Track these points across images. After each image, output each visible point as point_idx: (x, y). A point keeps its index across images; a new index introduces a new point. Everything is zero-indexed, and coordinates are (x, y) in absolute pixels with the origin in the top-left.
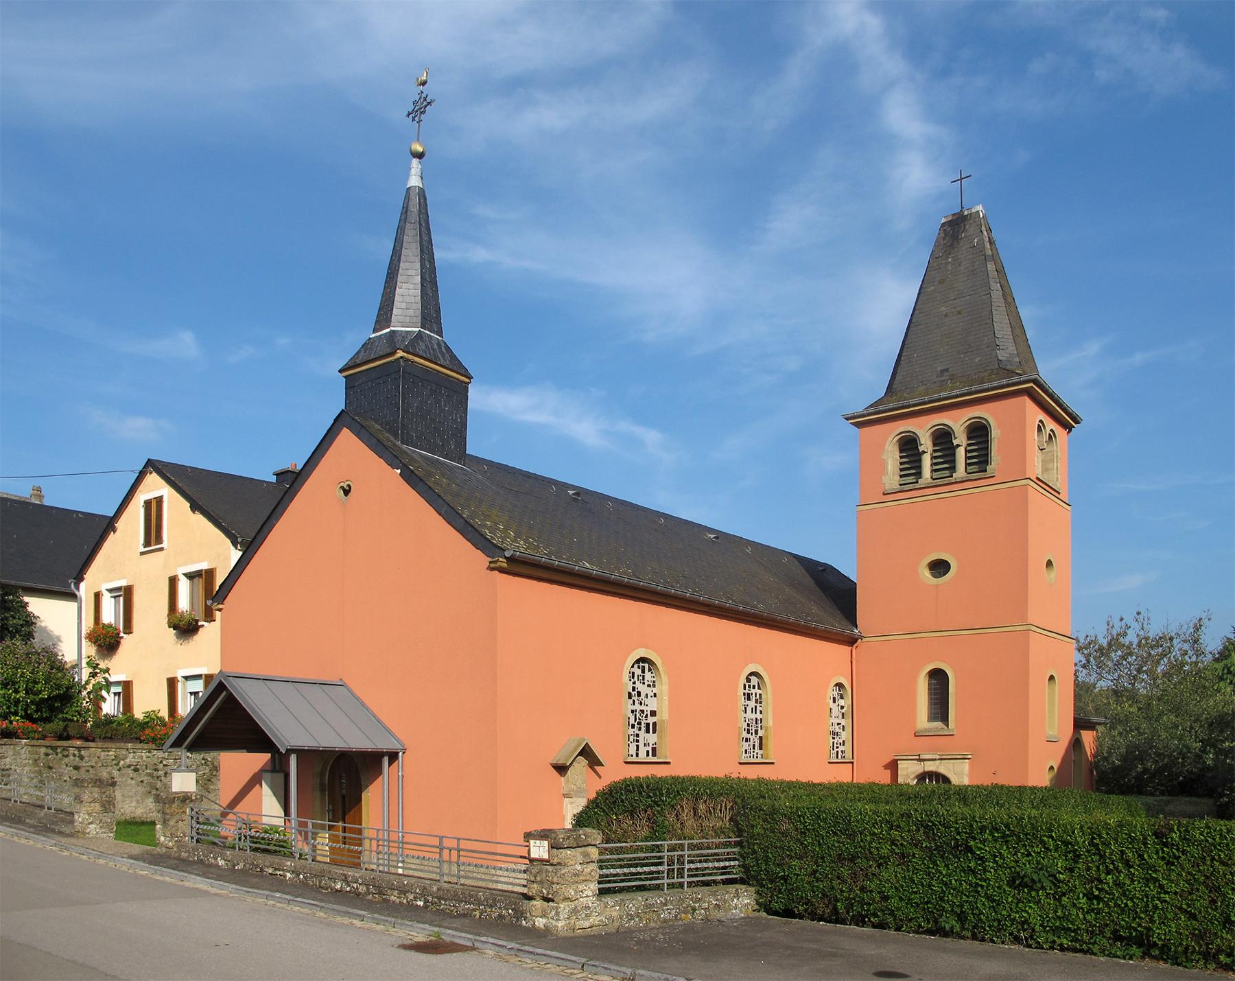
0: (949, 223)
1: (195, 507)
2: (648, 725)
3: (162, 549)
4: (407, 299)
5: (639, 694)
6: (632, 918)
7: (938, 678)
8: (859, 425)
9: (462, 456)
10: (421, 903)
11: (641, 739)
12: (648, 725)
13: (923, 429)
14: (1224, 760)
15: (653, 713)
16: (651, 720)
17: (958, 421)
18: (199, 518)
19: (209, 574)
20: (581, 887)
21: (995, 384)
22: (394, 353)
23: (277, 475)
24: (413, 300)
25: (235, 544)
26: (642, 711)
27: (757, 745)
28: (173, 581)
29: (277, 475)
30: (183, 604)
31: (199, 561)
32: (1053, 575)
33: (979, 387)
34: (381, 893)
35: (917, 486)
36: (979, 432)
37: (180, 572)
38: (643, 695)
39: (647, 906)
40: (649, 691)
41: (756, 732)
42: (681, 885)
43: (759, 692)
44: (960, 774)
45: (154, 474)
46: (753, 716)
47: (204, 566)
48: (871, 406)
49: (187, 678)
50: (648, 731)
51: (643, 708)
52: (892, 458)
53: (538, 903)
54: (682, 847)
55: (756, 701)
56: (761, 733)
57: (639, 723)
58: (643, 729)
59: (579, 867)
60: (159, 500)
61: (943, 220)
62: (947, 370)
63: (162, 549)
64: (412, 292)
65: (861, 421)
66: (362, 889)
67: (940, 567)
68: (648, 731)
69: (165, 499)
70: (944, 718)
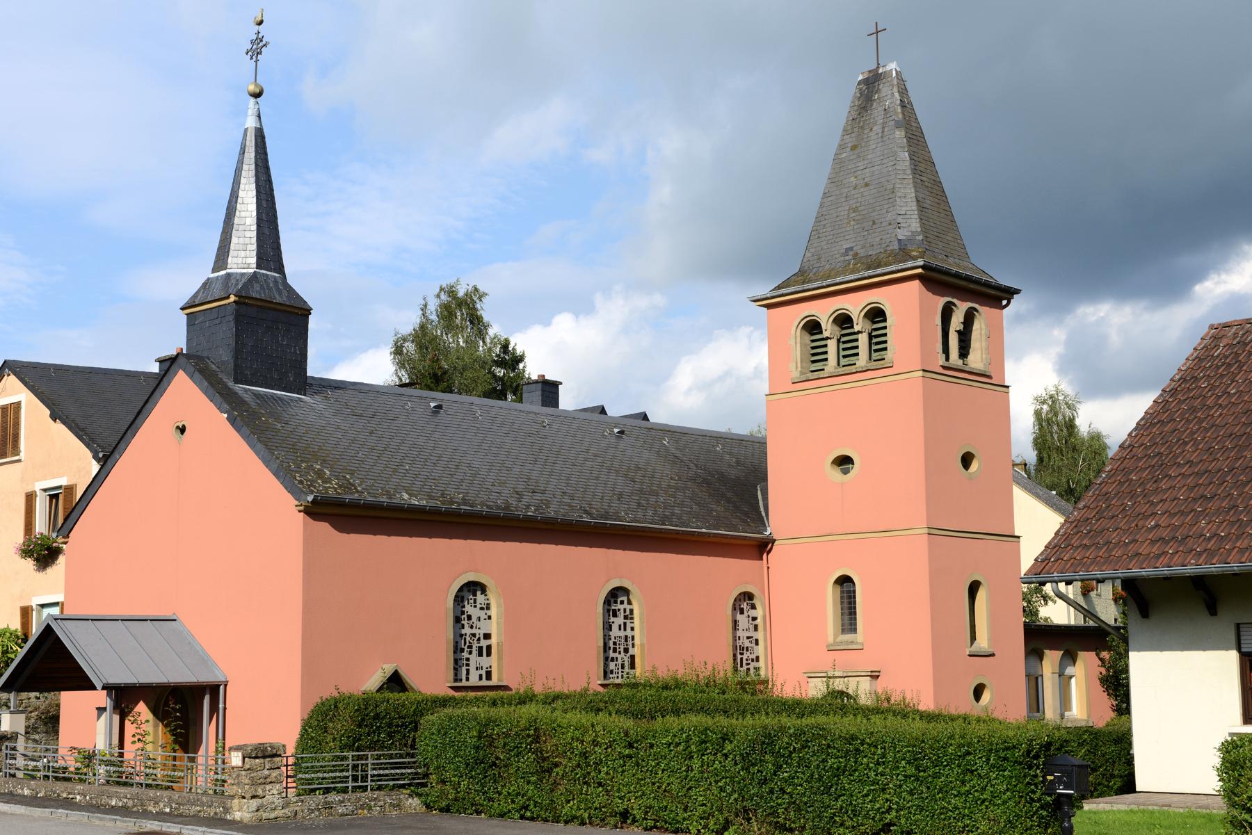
0: (866, 81)
1: (54, 417)
2: (480, 649)
3: (19, 461)
5: (469, 617)
8: (769, 306)
9: (303, 384)
10: (168, 810)
11: (472, 663)
12: (480, 649)
13: (824, 311)
15: (487, 636)
16: (484, 643)
17: (855, 305)
18: (60, 429)
19: (70, 489)
20: (268, 787)
21: (894, 268)
22: (228, 297)
23: (161, 361)
24: (247, 241)
25: (95, 457)
26: (474, 635)
27: (627, 664)
28: (30, 498)
29: (161, 361)
30: (41, 526)
31: (58, 476)
32: (835, 474)
33: (872, 272)
34: (142, 805)
36: (876, 315)
37: (38, 486)
38: (474, 619)
39: (326, 803)
40: (482, 614)
41: (626, 651)
42: (364, 789)
43: (628, 607)
44: (863, 690)
45: (12, 377)
46: (622, 634)
47: (63, 481)
48: (779, 287)
49: (43, 606)
50: (480, 654)
51: (474, 631)
52: (796, 342)
53: (236, 801)
55: (626, 617)
56: (631, 652)
57: (470, 647)
58: (475, 652)
59: (267, 772)
60: (17, 406)
61: (861, 78)
62: (851, 249)
63: (19, 461)
66: (130, 803)
67: (844, 462)
68: (480, 654)
69: (23, 405)
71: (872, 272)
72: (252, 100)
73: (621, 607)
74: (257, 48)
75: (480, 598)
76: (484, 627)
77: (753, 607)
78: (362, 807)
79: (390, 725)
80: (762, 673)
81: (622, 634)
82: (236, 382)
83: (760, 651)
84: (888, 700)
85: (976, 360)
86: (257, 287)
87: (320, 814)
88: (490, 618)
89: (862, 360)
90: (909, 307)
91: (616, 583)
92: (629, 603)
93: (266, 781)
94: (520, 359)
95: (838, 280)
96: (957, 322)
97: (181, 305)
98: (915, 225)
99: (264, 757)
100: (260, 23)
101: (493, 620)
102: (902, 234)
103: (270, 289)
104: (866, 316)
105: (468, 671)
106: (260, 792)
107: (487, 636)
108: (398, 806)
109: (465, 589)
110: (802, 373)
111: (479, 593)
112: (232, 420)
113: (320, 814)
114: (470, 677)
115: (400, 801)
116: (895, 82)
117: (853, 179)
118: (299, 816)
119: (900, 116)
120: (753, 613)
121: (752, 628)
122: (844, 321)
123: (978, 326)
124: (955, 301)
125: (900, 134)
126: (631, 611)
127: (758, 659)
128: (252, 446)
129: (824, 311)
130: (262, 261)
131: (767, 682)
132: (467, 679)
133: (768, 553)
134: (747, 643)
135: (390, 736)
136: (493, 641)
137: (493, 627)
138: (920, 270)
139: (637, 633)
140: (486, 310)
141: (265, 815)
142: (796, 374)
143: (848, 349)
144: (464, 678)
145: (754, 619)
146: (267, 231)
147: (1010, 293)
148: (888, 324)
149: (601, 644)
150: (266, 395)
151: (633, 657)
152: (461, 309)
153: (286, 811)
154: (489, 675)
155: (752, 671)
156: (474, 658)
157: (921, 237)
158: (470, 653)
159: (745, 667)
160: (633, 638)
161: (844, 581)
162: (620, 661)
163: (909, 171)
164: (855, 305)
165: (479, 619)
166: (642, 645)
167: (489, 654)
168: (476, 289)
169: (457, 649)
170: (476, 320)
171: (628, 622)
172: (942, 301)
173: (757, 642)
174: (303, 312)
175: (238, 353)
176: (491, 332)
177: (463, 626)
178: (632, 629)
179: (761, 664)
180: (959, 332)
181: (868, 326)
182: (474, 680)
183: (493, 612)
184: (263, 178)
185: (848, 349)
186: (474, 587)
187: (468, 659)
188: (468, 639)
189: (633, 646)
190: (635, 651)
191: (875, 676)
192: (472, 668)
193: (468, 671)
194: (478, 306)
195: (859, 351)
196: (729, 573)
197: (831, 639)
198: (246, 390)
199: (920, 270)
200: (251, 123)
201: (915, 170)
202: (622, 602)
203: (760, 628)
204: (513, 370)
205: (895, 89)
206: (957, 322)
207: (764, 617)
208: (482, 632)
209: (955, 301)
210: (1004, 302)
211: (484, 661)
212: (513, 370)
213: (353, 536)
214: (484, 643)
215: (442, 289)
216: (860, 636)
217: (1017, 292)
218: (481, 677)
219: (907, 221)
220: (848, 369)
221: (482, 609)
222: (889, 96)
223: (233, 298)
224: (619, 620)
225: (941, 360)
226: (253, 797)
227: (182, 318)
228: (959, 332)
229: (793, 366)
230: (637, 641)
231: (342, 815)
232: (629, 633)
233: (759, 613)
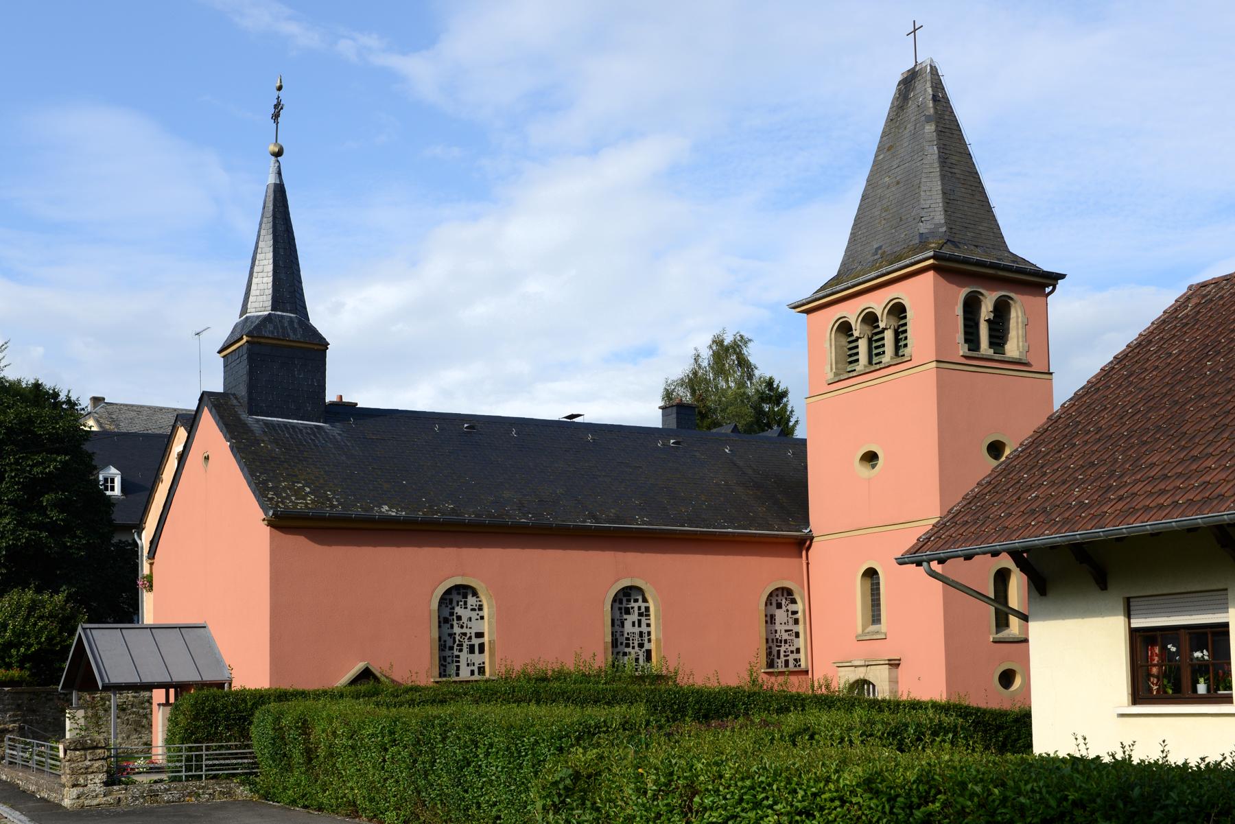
4: (261, 287)
6: (137, 799)
7: (871, 574)
8: (808, 312)
13: (851, 311)
14: (1177, 653)
15: (480, 635)
16: (476, 642)
17: (878, 302)
20: (90, 777)
21: (907, 262)
22: (241, 338)
23: (803, 442)
26: (465, 634)
29: (803, 442)
32: (864, 471)
33: (896, 266)
35: (854, 374)
36: (898, 310)
38: (464, 619)
40: (474, 615)
41: (641, 646)
43: (643, 605)
48: (822, 288)
51: (464, 630)
52: (828, 345)
54: (200, 749)
55: (640, 615)
56: (647, 646)
57: (461, 645)
62: (880, 248)
64: (265, 280)
65: (809, 307)
67: (870, 458)
70: (876, 619)
71: (896, 266)
72: (273, 158)
73: (636, 605)
75: (471, 600)
76: (476, 627)
77: (794, 601)
78: (190, 795)
79: (227, 718)
80: (803, 663)
81: (636, 630)
82: (251, 413)
83: (801, 643)
84: (827, 687)
85: (1013, 348)
86: (270, 327)
87: (145, 801)
88: (482, 618)
89: (886, 359)
90: (922, 295)
91: (626, 582)
92: (645, 600)
93: (87, 771)
94: (785, 394)
95: (861, 279)
96: (986, 310)
97: (218, 349)
98: (940, 217)
99: (85, 749)
101: (484, 620)
102: (923, 228)
103: (283, 327)
104: (890, 312)
107: (480, 635)
108: (229, 793)
109: (454, 592)
110: (836, 374)
111: (470, 597)
112: (232, 448)
113: (145, 801)
115: (231, 789)
116: (929, 78)
117: (887, 179)
118: (123, 803)
119: (932, 111)
120: (792, 607)
121: (791, 621)
122: (870, 319)
123: (1016, 316)
124: (1012, 295)
125: (930, 128)
126: (647, 609)
127: (798, 651)
128: (242, 470)
130: (277, 303)
131: (806, 672)
132: (458, 675)
133: (808, 549)
134: (785, 636)
135: (228, 728)
136: (486, 639)
137: (485, 627)
138: (931, 261)
139: (652, 629)
140: (753, 354)
141: (86, 803)
142: (830, 376)
144: (453, 672)
145: (795, 613)
146: (283, 276)
147: (1054, 278)
148: (907, 320)
149: (609, 639)
150: (279, 424)
151: (649, 652)
153: (108, 798)
154: (481, 670)
155: (791, 663)
156: (464, 656)
157: (944, 229)
158: (461, 650)
159: (783, 659)
160: (649, 633)
161: (871, 574)
162: (633, 656)
163: (936, 165)
164: (878, 302)
165: (470, 619)
166: (657, 640)
167: (482, 650)
168: (742, 337)
169: (443, 646)
170: (743, 363)
171: (643, 619)
172: (963, 292)
173: (797, 635)
175: (251, 387)
176: (757, 373)
177: (452, 626)
178: (648, 625)
179: (802, 656)
180: (988, 321)
181: (894, 323)
182: (465, 674)
183: (485, 612)
184: (281, 228)
186: (464, 591)
187: (458, 657)
188: (457, 638)
189: (649, 641)
190: (653, 646)
191: (894, 664)
192: (463, 664)
193: (458, 668)
194: (744, 351)
195: (886, 349)
196: (767, 571)
197: (860, 630)
198: (258, 421)
199: (931, 261)
200: (272, 179)
201: (944, 160)
202: (636, 601)
203: (801, 622)
204: (778, 405)
205: (929, 84)
206: (986, 310)
207: (804, 611)
208: (473, 631)
209: (1012, 295)
210: (1048, 290)
211: (477, 658)
212: (778, 405)
213: (646, 555)
214: (476, 642)
215: (714, 342)
216: (883, 627)
217: (1062, 276)
218: (472, 673)
219: (932, 212)
220: (878, 367)
221: (473, 610)
222: (924, 91)
223: (245, 338)
224: (634, 617)
225: (963, 349)
226: (74, 786)
227: (220, 361)
228: (988, 321)
230: (653, 637)
231: (168, 802)
232: (644, 629)
233: (799, 607)
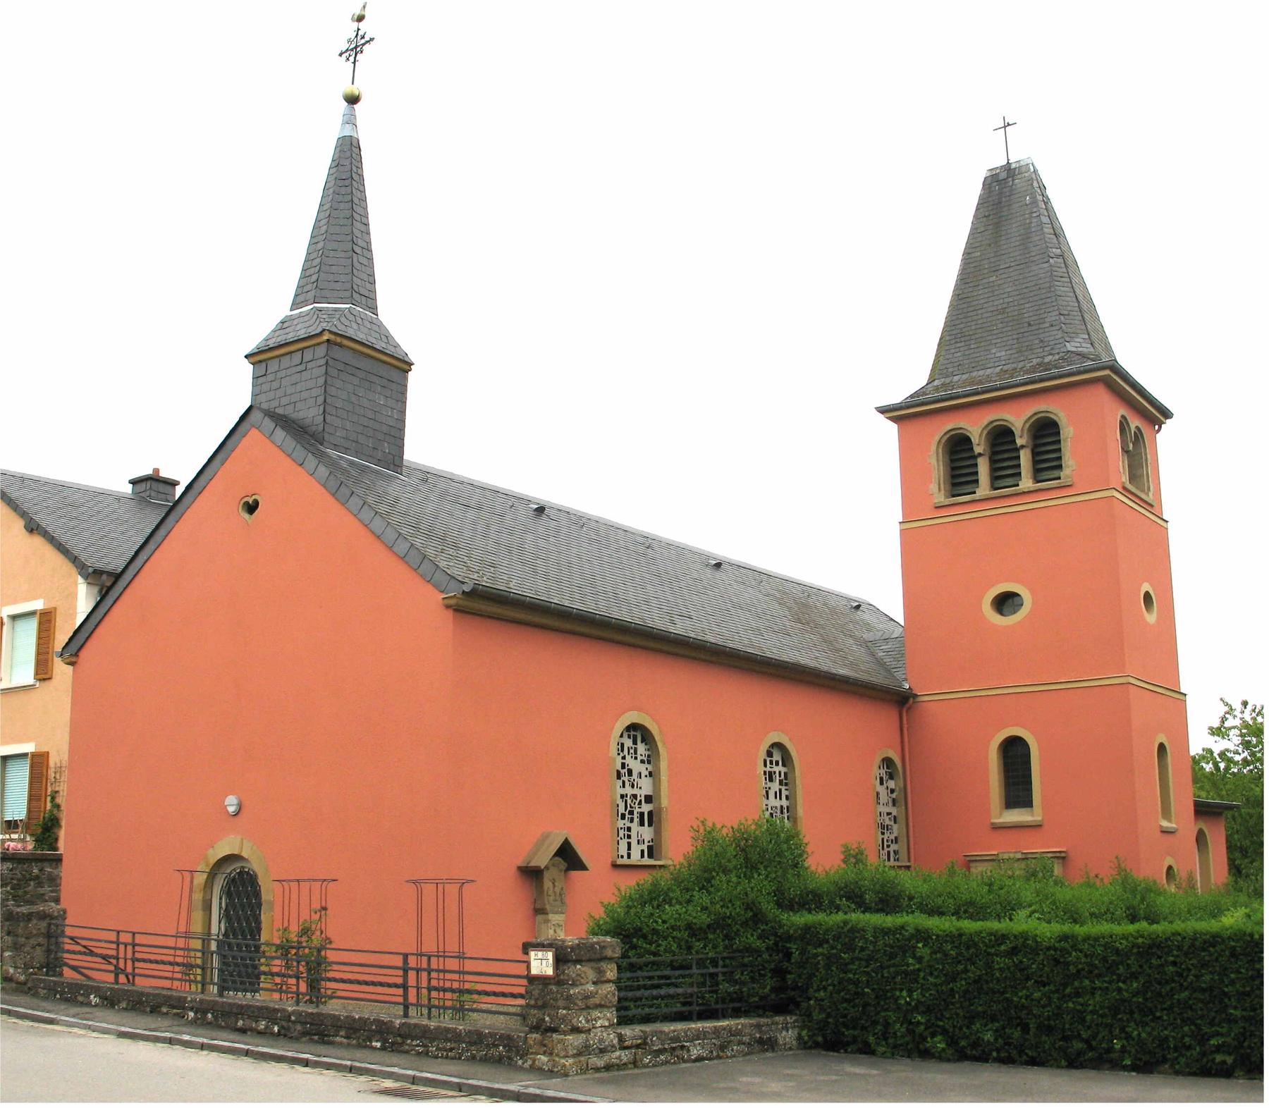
5: (630, 772)
16: (646, 808)
26: (635, 796)
51: (635, 791)
52: (935, 464)
57: (631, 813)
58: (636, 820)
59: (592, 988)
68: (642, 824)
74: (355, 49)
100: (360, 19)
105: (629, 844)
106: (582, 1022)
114: (632, 852)
122: (1001, 437)
129: (975, 427)
132: (629, 856)
143: (1004, 472)
152: (247, 503)
158: (632, 820)
164: (1018, 418)
174: (403, 366)
185: (1004, 472)
192: (634, 841)
193: (629, 844)
227: (248, 368)
229: (933, 487)
